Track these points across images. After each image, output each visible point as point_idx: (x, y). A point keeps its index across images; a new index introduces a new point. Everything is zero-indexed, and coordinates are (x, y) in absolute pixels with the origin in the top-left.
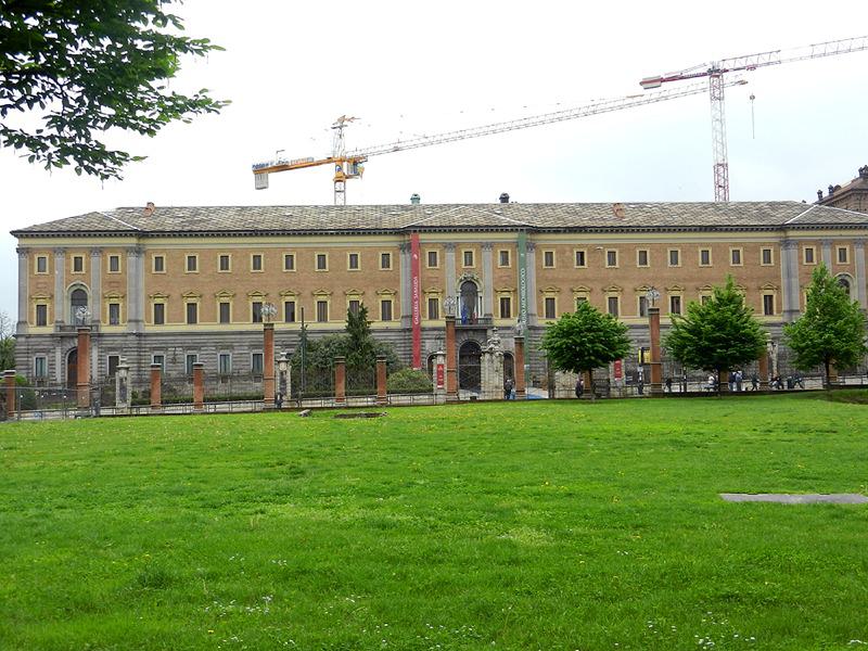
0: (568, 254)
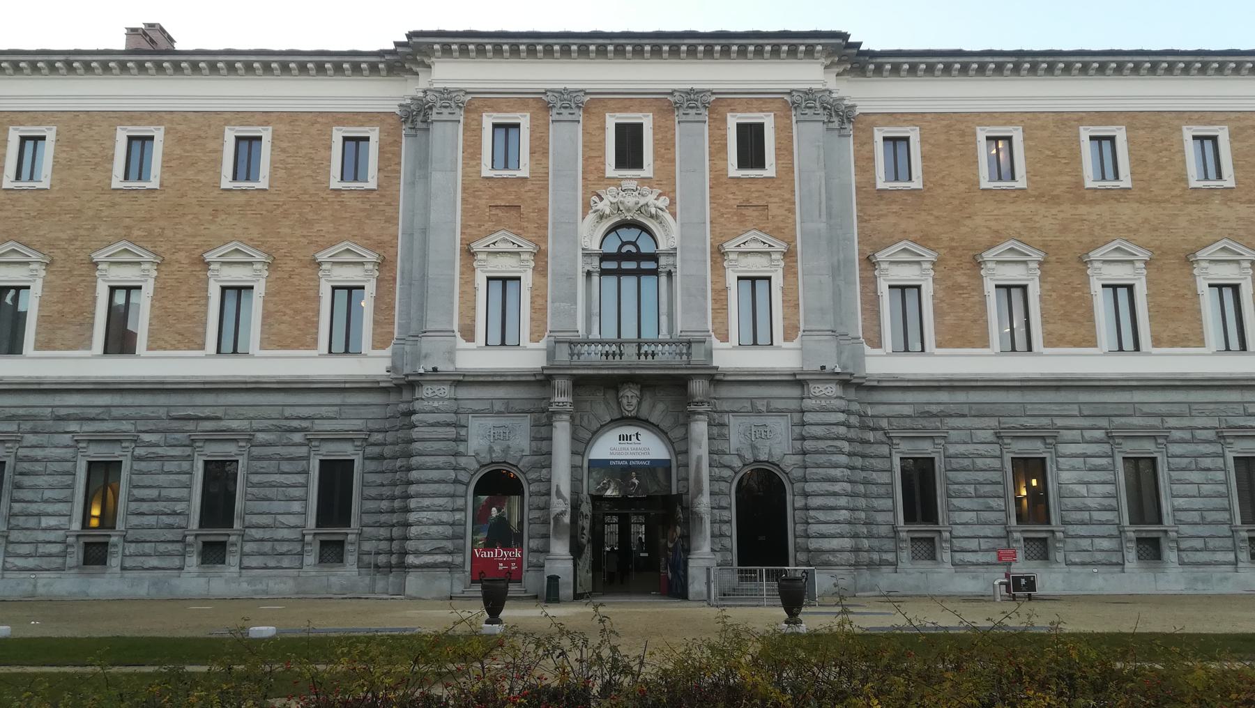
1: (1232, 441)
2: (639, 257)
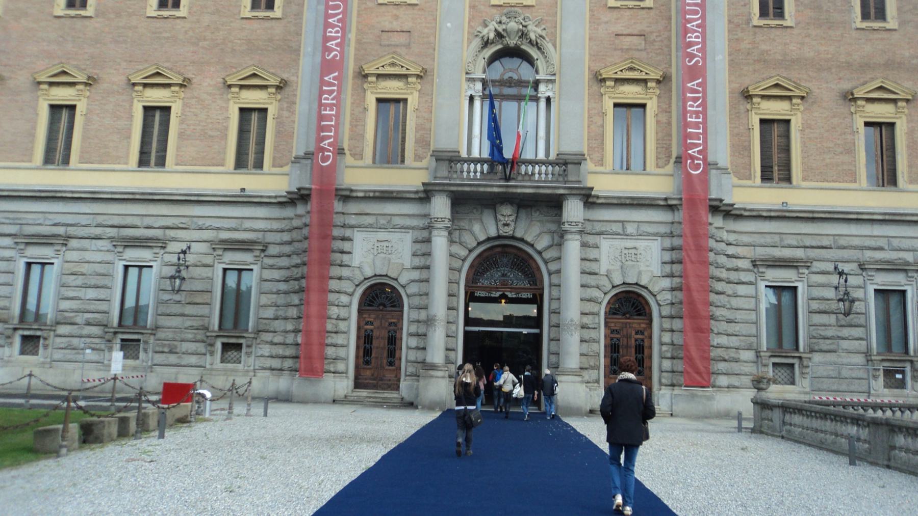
1: (873, 273)
2: (521, 83)
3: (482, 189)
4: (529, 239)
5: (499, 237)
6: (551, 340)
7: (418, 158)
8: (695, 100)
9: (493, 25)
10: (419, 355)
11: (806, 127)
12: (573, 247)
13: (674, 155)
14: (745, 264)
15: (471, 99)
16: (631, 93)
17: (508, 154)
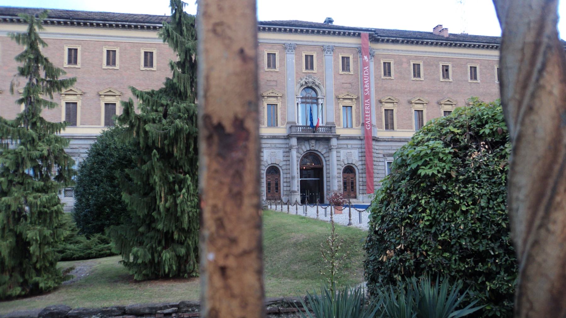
0: (405, 65)
3: (307, 136)
4: (320, 151)
5: (310, 150)
6: (327, 182)
7: (282, 124)
8: (367, 106)
9: (304, 80)
10: (288, 188)
11: (398, 111)
12: (334, 153)
13: (361, 122)
14: (381, 156)
15: (298, 104)
16: (348, 103)
17: (315, 124)
